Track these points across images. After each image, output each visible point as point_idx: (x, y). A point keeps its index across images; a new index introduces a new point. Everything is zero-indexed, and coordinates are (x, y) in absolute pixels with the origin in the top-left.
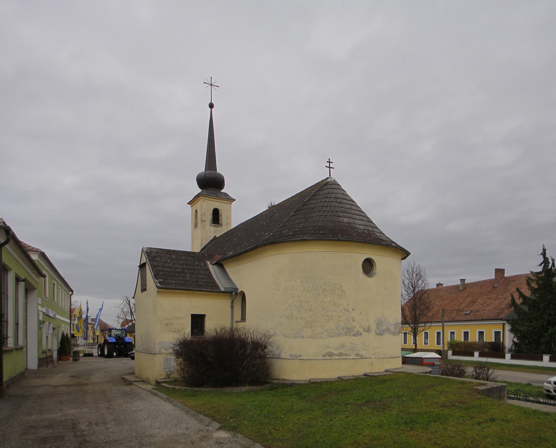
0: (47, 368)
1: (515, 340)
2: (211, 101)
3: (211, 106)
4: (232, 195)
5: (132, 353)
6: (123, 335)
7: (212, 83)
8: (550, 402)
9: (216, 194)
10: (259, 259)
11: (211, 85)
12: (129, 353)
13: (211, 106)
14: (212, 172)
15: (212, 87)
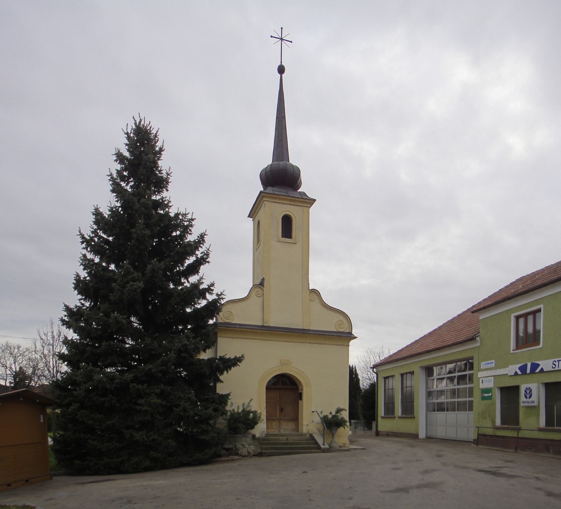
0: (512, 350)
1: (217, 383)
2: (281, 63)
3: (281, 70)
4: (310, 195)
5: (355, 368)
6: (94, 258)
7: (281, 41)
8: (518, 435)
9: (287, 193)
10: (245, 339)
11: (282, 39)
12: (26, 381)
13: (281, 70)
14: (281, 163)
15: (282, 42)
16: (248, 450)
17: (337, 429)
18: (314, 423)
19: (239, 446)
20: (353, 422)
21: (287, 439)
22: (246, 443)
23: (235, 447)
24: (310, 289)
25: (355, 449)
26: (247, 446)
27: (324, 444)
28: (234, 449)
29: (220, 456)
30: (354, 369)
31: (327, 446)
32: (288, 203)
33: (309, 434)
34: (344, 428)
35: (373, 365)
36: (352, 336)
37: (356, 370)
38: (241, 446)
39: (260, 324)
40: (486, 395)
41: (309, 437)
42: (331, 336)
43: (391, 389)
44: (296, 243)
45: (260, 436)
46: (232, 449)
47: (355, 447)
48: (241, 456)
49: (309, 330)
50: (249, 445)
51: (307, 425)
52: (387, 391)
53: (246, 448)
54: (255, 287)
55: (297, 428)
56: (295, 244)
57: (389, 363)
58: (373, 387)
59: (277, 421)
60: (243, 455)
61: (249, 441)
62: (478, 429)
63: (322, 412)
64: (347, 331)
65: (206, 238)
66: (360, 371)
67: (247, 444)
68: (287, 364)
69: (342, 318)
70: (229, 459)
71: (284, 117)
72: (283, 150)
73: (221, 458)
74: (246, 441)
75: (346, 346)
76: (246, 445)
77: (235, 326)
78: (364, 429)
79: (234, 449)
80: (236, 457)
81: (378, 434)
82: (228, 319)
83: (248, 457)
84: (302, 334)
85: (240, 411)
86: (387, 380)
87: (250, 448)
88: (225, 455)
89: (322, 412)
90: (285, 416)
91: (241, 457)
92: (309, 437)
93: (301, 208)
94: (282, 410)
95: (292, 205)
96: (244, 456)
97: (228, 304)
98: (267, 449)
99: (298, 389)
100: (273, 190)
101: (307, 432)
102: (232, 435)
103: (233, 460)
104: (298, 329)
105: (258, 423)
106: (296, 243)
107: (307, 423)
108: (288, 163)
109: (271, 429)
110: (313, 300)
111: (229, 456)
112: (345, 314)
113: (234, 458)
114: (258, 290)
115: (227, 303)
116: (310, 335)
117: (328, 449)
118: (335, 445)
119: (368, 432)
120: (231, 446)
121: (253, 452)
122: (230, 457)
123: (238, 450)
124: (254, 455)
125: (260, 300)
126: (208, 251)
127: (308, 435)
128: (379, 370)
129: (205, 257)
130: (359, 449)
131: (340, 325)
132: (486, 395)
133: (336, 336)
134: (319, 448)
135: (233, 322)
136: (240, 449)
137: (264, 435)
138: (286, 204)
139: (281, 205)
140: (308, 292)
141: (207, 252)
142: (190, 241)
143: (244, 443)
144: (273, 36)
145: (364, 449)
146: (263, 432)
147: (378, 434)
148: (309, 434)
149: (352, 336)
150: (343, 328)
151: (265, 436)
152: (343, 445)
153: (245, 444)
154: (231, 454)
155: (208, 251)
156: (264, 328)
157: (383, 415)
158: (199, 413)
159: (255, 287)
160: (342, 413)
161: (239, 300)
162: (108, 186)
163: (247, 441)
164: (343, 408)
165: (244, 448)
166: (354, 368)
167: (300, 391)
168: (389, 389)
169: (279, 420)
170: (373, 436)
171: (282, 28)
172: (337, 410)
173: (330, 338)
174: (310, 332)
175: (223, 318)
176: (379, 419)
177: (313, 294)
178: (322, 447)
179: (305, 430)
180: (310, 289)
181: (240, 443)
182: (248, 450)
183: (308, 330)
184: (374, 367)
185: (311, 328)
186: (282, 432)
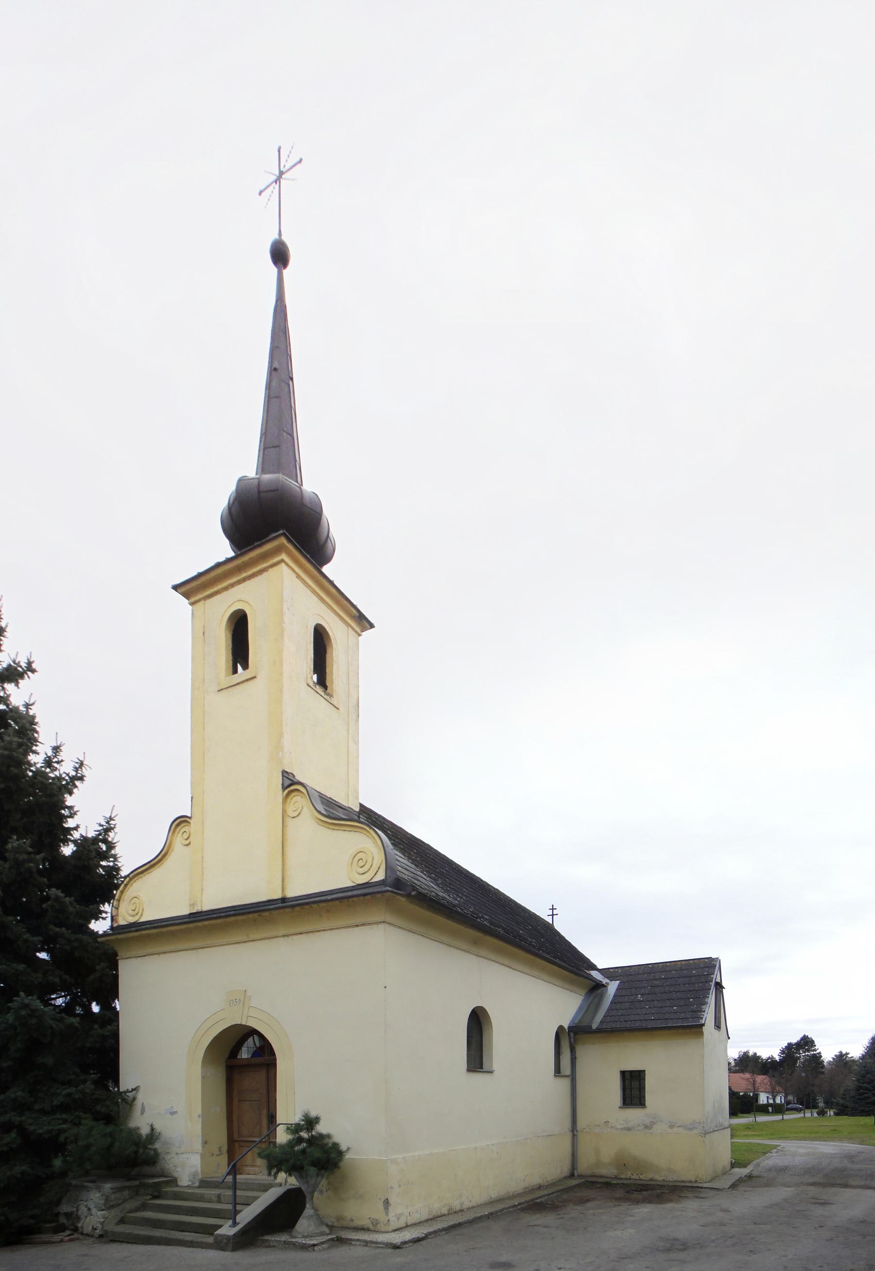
45: (190, 1183)
48: (82, 1234)
56: (255, 679)
106: (255, 677)
135: (143, 919)
138: (232, 585)
139: (225, 594)
151: (199, 1187)
152: (371, 1227)
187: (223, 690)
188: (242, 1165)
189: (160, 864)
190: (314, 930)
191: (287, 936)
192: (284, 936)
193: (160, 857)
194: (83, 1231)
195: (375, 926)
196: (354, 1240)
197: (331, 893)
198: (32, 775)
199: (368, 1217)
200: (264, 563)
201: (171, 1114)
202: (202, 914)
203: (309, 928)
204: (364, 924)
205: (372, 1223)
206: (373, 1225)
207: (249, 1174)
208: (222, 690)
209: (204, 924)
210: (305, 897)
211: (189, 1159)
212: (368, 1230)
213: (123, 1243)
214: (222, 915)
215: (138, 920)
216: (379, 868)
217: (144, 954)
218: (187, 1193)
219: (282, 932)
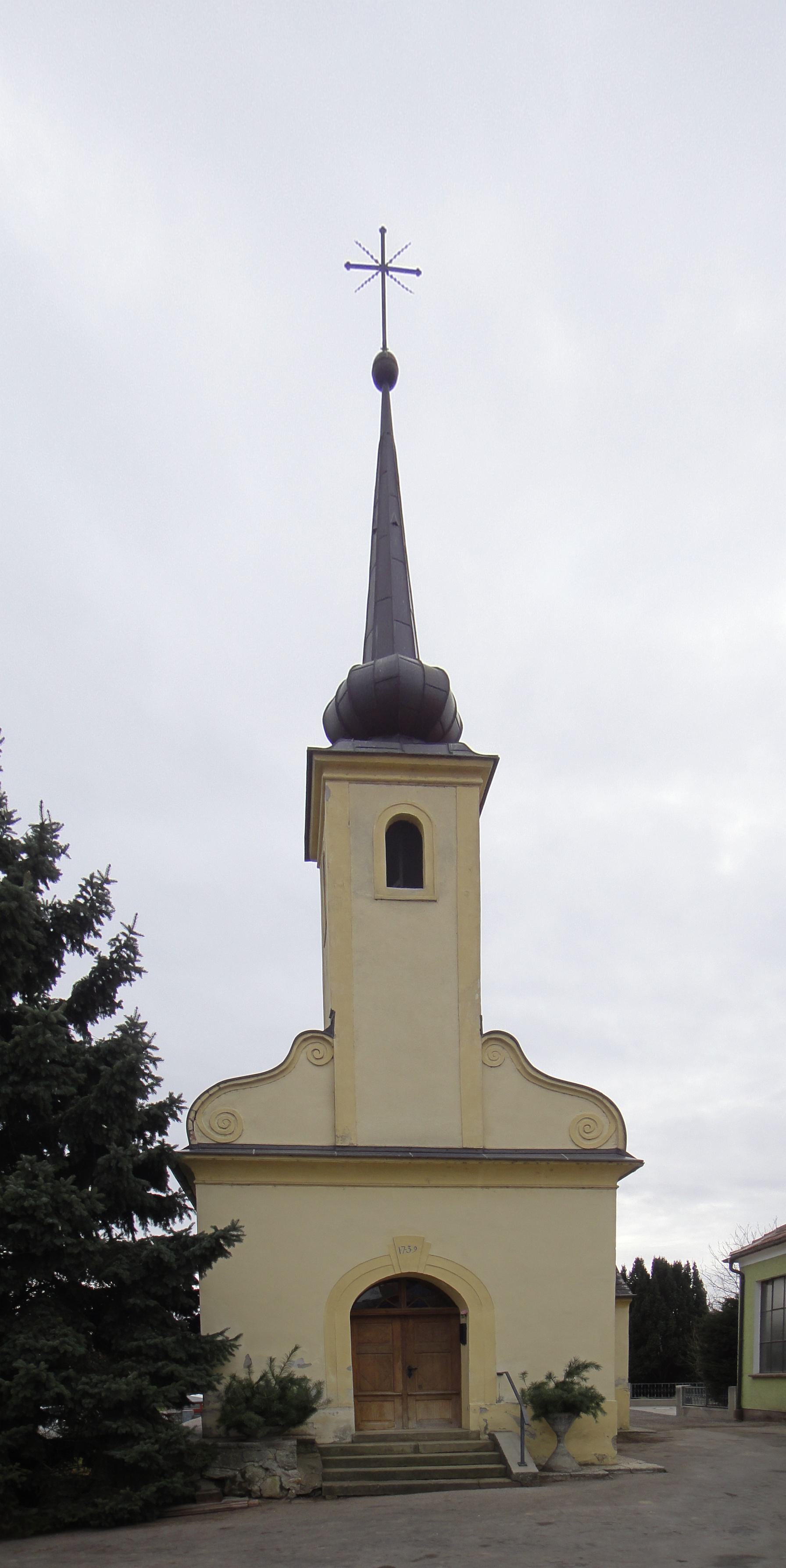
2: (384, 347)
5: (693, 1268)
11: (384, 268)
16: (281, 1481)
17: (570, 1421)
18: (502, 1403)
19: (253, 1470)
20: (679, 1389)
21: (416, 1449)
22: (276, 1465)
23: (243, 1474)
24: (484, 1033)
25: (631, 1471)
26: (279, 1471)
27: (522, 1463)
28: (239, 1478)
29: (193, 1500)
30: (692, 1271)
31: (532, 1469)
32: (406, 778)
33: (489, 1435)
34: (595, 1416)
35: (732, 1255)
36: (627, 1158)
37: (696, 1273)
38: (261, 1472)
39: (325, 1141)
40: (697, 1391)
41: (489, 1441)
42: (552, 1163)
43: (782, 1308)
44: (435, 901)
45: (337, 1440)
46: (233, 1479)
47: (634, 1464)
48: (261, 1497)
49: (484, 1150)
50: (286, 1467)
51: (483, 1410)
52: (769, 1315)
53: (277, 1478)
54: (305, 1040)
55: (457, 1417)
56: (435, 903)
57: (777, 1244)
58: (733, 1307)
59: (398, 1401)
60: (266, 1494)
61: (284, 1459)
62: (772, 1313)
63: (524, 1374)
64: (611, 1146)
65: (114, 893)
66: (717, 1278)
67: (279, 1466)
68: (416, 1248)
69: (593, 1110)
70: (221, 1507)
71: (395, 524)
72: (393, 624)
73: (194, 1506)
74: (275, 1459)
75: (612, 1188)
76: (274, 1468)
77: (248, 1151)
78: (707, 1402)
79: (239, 1478)
80: (243, 1502)
81: (741, 1415)
82: (225, 1135)
83: (283, 1500)
84: (459, 1162)
85: (255, 1378)
86: (770, 1287)
87: (287, 1475)
88: (210, 1498)
89: (524, 1374)
90: (420, 1387)
91: (257, 1501)
92: (489, 1441)
93: (450, 790)
94: (410, 1372)
95: (419, 783)
96: (271, 1498)
97: (223, 1092)
98: (342, 1477)
99: (458, 1315)
100: (353, 744)
101: (483, 1429)
102: (232, 1444)
103: (232, 1510)
104: (448, 1150)
105: (314, 1410)
106: (435, 901)
107: (482, 1404)
108: (412, 660)
109: (380, 1421)
110: (494, 1059)
111: (220, 1500)
112: (601, 1098)
113: (234, 1505)
114: (317, 1046)
115: (220, 1089)
116: (485, 1162)
117: (534, 1476)
118: (564, 1463)
119: (718, 1412)
120: (230, 1473)
121: (297, 1487)
122: (223, 1501)
123: (250, 1481)
124: (299, 1496)
125: (323, 1074)
126: (132, 936)
127: (487, 1436)
128: (746, 1264)
129: (125, 953)
130: (645, 1470)
131: (587, 1129)
132: (697, 1391)
133: (570, 1161)
134: (506, 1472)
135: (241, 1141)
136: (257, 1479)
137: (349, 1439)
138: (399, 783)
139: (384, 787)
140: (479, 1042)
141: (129, 939)
142: (60, 903)
143: (267, 1464)
144: (352, 263)
145: (664, 1471)
146: (344, 1431)
147: (741, 1415)
148: (489, 1435)
149: (627, 1158)
150: (496, 1060)
151: (353, 1442)
152: (596, 1462)
153: (273, 1466)
154: (231, 1494)
155: (132, 936)
156: (338, 1151)
157: (756, 1370)
158: (91, 1391)
159: (305, 1040)
160: (585, 1374)
161: (256, 1078)
162: (140, 950)
163: (278, 1458)
164: (588, 1361)
165: (270, 1476)
166: (691, 1267)
167: (462, 1321)
168: (774, 1308)
169: (404, 1397)
170: (729, 1421)
171: (383, 231)
172: (570, 1366)
173: (552, 1170)
174: (485, 1156)
175: (209, 1131)
176: (746, 1381)
177: (497, 1047)
178: (516, 1469)
179: (474, 1422)
180: (484, 1033)
181: (256, 1464)
182: (281, 1481)
183: (481, 1151)
184: (733, 1258)
185: (490, 1146)
186: (413, 1428)
187: (383, 901)
188: (362, 1421)
189: (272, 1080)
190: (244, 1183)
191: (487, 1187)
192: (482, 1187)
193: (277, 1072)
194: (261, 1495)
195: (605, 1191)
196: (615, 1471)
197: (607, 1152)
198: (82, 916)
199: (594, 1453)
200: (432, 777)
201: (298, 1367)
202: (356, 1149)
203: (585, 1183)
204: (592, 1187)
205: (598, 1458)
206: (599, 1460)
207: (374, 1430)
208: (382, 899)
209: (233, 1159)
210: (495, 1151)
211: (335, 1414)
212: (593, 1464)
213: (350, 1499)
214: (399, 1155)
215: (233, 1142)
216: (611, 1137)
217: (249, 1183)
218: (367, 1447)
219: (480, 1182)
